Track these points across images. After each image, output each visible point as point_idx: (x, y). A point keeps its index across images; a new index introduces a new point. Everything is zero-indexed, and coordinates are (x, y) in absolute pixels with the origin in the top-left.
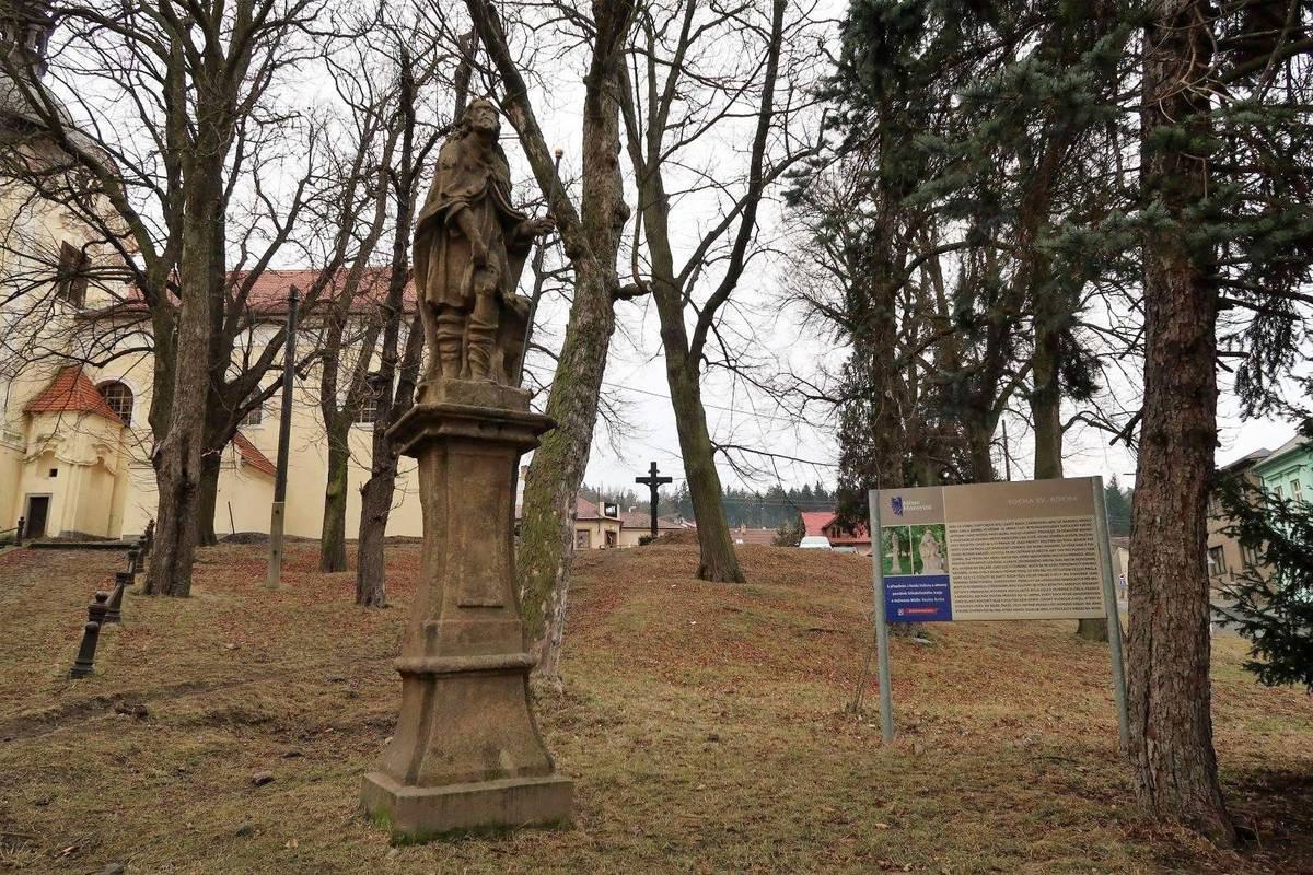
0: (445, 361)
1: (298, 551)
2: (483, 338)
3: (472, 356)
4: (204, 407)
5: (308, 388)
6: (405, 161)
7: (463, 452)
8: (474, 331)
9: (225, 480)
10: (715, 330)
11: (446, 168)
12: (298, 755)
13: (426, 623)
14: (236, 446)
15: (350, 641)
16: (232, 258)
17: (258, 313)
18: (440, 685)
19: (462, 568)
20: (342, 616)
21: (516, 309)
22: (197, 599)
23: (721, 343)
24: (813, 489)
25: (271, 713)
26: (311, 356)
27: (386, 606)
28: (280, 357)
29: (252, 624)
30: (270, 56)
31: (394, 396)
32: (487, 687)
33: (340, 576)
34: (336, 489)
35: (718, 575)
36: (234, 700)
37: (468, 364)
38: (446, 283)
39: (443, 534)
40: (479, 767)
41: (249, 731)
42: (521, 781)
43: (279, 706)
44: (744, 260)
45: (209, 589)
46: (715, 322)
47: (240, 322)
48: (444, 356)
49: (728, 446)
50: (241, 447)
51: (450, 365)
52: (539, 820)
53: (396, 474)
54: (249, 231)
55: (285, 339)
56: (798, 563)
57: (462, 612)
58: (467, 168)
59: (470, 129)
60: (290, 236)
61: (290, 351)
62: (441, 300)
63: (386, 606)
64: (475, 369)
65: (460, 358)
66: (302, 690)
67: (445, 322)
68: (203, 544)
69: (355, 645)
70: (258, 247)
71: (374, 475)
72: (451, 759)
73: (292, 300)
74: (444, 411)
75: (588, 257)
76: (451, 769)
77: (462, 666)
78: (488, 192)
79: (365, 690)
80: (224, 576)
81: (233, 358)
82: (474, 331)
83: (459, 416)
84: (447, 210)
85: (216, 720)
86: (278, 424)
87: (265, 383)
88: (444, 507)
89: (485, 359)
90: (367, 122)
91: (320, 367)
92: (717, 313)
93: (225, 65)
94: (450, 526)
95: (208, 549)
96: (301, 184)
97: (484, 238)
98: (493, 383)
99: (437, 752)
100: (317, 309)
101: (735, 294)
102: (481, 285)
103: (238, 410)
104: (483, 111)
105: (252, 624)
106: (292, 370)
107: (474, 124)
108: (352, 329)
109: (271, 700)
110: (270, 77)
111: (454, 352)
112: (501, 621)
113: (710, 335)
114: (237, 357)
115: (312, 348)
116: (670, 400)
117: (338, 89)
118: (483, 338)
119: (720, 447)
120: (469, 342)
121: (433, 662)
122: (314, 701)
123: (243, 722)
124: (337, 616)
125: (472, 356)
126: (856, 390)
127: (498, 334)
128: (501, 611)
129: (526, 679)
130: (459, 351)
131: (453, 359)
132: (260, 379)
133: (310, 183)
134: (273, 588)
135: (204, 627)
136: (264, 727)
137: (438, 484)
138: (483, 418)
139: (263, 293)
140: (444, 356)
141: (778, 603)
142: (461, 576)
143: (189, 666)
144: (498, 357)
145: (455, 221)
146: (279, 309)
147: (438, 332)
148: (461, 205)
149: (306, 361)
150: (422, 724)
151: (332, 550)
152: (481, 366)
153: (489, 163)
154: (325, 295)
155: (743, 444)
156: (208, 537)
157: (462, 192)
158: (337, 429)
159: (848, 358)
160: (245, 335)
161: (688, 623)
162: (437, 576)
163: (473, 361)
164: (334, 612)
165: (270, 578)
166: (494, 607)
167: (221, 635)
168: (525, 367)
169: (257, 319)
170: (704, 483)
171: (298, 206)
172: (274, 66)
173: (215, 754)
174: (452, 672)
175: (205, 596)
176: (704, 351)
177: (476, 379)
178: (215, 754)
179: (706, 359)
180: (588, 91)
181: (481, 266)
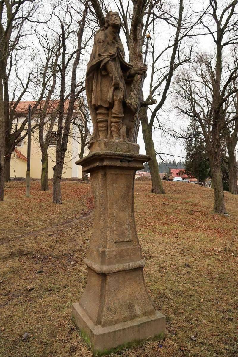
0: (101, 131)
1: (34, 184)
2: (118, 120)
3: (113, 129)
4: (4, 143)
5: (35, 135)
6: (63, 62)
7: (113, 173)
8: (114, 117)
9: (12, 162)
10: (157, 117)
12: (41, 272)
13: (101, 250)
14: (15, 152)
15: (53, 217)
16: (11, 98)
17: (19, 114)
18: (108, 278)
19: (114, 225)
20: (49, 207)
21: (132, 107)
22: (5, 201)
23: (158, 122)
24: (172, 162)
25: (31, 250)
26: (35, 126)
27: (62, 203)
28: (26, 127)
29: (23, 211)
30: (18, 33)
31: (62, 137)
32: (127, 277)
33: (47, 192)
34: (44, 166)
35: (157, 192)
36: (17, 246)
38: (101, 96)
39: (106, 209)
40: (127, 314)
41: (24, 258)
42: (145, 319)
43: (33, 247)
45: (10, 198)
46: (157, 115)
47: (14, 116)
48: (100, 129)
49: (160, 153)
50: (16, 152)
51: (103, 133)
52: (153, 336)
53: (63, 163)
54: (15, 89)
55: (28, 120)
56: (178, 187)
57: (116, 245)
58: (108, 43)
60: (27, 90)
61: (29, 125)
62: (99, 104)
63: (62, 203)
64: (115, 135)
65: (107, 129)
66: (40, 240)
67: (100, 114)
68: (7, 181)
69: (54, 218)
70: (18, 94)
71: (57, 163)
72: (115, 312)
73: (29, 109)
74: (106, 155)
75: (133, 91)
76: (116, 317)
77: (117, 269)
78: (117, 55)
79: (61, 239)
80: (14, 193)
81: (13, 127)
82: (114, 117)
83: (108, 157)
84: (101, 61)
85: (12, 255)
86: (27, 147)
87: (22, 134)
88: (105, 197)
89: (119, 130)
90: (48, 54)
91: (38, 130)
92: (157, 112)
93: (4, 32)
94: (109, 206)
95: (9, 183)
96: (30, 74)
97: (118, 75)
98: (124, 141)
99: (109, 309)
100: (36, 112)
102: (117, 97)
103: (15, 142)
104: (114, 16)
105: (23, 211)
106: (30, 131)
108: (48, 118)
109: (31, 246)
110: (19, 40)
111: (105, 127)
112: (132, 247)
113: (155, 119)
114: (14, 127)
115: (35, 124)
117: (40, 42)
118: (118, 120)
119: (158, 154)
120: (111, 122)
121: (105, 268)
122: (44, 244)
123: (21, 255)
124: (48, 207)
125: (113, 129)
126: (190, 135)
127: (123, 118)
128: (131, 242)
129: (142, 271)
130: (107, 127)
131: (104, 130)
132: (21, 133)
133: (32, 74)
134: (28, 197)
135: (8, 212)
136: (29, 256)
137: (102, 187)
138: (122, 158)
139: (20, 108)
140: (100, 129)
141: (177, 200)
142: (115, 229)
143: (3, 230)
144: (123, 129)
145: (105, 67)
146: (25, 112)
147: (98, 118)
148: (108, 59)
149: (34, 128)
150: (101, 295)
151: (44, 184)
153: (117, 41)
154: (39, 108)
155: (165, 153)
156: (8, 179)
157: (107, 54)
158: (44, 149)
159: (189, 126)
160: (16, 120)
161: (154, 209)
162: (104, 228)
163: (114, 131)
164: (47, 206)
165: (27, 193)
166: (128, 241)
167: (13, 216)
169: (19, 115)
170: (154, 164)
171: (29, 81)
172: (20, 37)
173: (12, 272)
174: (113, 273)
175: (8, 200)
176: (153, 124)
177: (115, 139)
178: (12, 272)
179: (154, 127)
180: (142, 21)
181: (117, 88)
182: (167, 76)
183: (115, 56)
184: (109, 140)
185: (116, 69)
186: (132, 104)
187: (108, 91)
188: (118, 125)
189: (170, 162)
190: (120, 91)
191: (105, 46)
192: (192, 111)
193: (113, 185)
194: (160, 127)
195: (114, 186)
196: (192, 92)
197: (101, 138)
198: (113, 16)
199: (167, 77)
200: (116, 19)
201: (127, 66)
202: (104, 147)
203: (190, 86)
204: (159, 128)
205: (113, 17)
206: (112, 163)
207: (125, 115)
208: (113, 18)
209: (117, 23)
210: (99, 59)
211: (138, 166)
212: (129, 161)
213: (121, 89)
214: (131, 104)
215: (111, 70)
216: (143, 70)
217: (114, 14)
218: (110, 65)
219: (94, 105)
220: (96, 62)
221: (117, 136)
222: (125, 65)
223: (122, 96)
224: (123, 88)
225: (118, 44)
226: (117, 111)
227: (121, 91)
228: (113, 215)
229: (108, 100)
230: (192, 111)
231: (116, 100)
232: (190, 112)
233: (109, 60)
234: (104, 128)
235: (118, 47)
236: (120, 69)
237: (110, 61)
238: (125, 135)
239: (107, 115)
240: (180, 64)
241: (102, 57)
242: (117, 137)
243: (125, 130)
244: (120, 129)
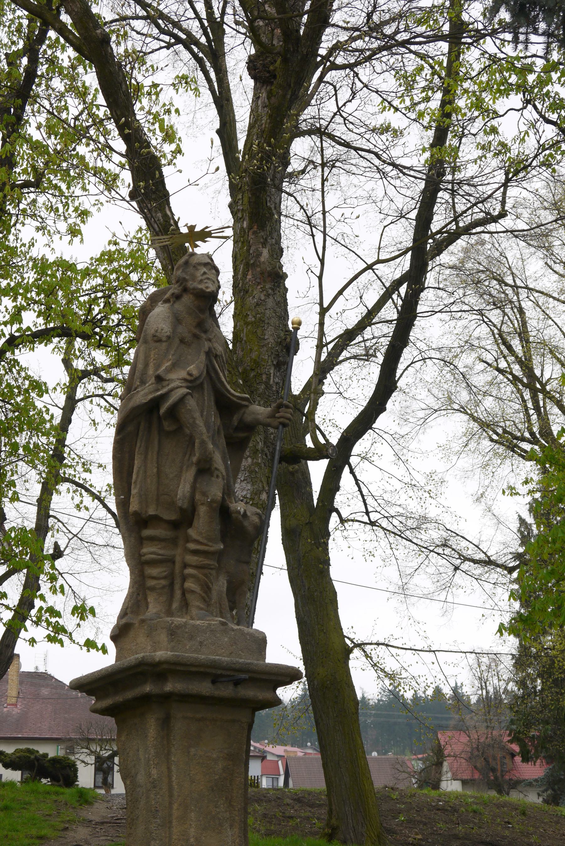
0: (152, 589)
2: (207, 562)
3: (190, 584)
8: (195, 552)
10: (352, 472)
11: (159, 341)
21: (246, 524)
23: (360, 490)
37: (183, 594)
44: (398, 375)
48: (151, 583)
58: (182, 341)
59: (185, 290)
62: (151, 511)
64: (195, 602)
67: (152, 539)
74: (175, 664)
82: (195, 552)
83: (179, 668)
89: (207, 589)
92: (358, 448)
94: (176, 813)
98: (223, 624)
101: (382, 422)
107: (191, 285)
111: (165, 578)
113: (346, 477)
116: (286, 573)
118: (207, 562)
119: (360, 646)
120: (185, 566)
125: (190, 584)
130: (171, 577)
131: (164, 587)
138: (219, 672)
145: (173, 412)
147: (144, 550)
152: (203, 598)
153: (205, 332)
157: (183, 374)
163: (193, 592)
168: (51, 513)
182: (397, 284)
183: (201, 380)
184: (178, 620)
185: (202, 416)
186: (249, 514)
187: (179, 476)
188: (205, 575)
189: (438, 691)
190: (213, 479)
191: (172, 352)
192: (532, 434)
193: (189, 752)
194: (367, 513)
195: (192, 754)
196: (531, 339)
197: (154, 611)
198: (199, 267)
199: (403, 290)
200: (208, 279)
201: (235, 399)
202: (166, 639)
203: (521, 311)
204: (366, 519)
205: (197, 270)
206: (190, 687)
207: (225, 547)
208: (199, 274)
209: (208, 290)
210: (158, 390)
211: (261, 698)
212: (237, 683)
213: (216, 473)
214: (245, 515)
215: (191, 421)
216: (282, 420)
217: (200, 264)
218: (189, 407)
219: (136, 513)
220: (150, 397)
221: (202, 606)
222: (229, 398)
223: (219, 494)
224: (222, 467)
225: (210, 340)
226: (204, 535)
227: (218, 477)
228: (188, 840)
229: (180, 503)
230: (532, 434)
231: (202, 504)
232: (523, 439)
233: (188, 394)
234: (163, 582)
235: (210, 349)
236: (213, 411)
237: (189, 397)
238: (226, 603)
239: (174, 542)
240: (428, 288)
241: (165, 383)
242: (202, 609)
243: (225, 589)
244: (210, 584)
